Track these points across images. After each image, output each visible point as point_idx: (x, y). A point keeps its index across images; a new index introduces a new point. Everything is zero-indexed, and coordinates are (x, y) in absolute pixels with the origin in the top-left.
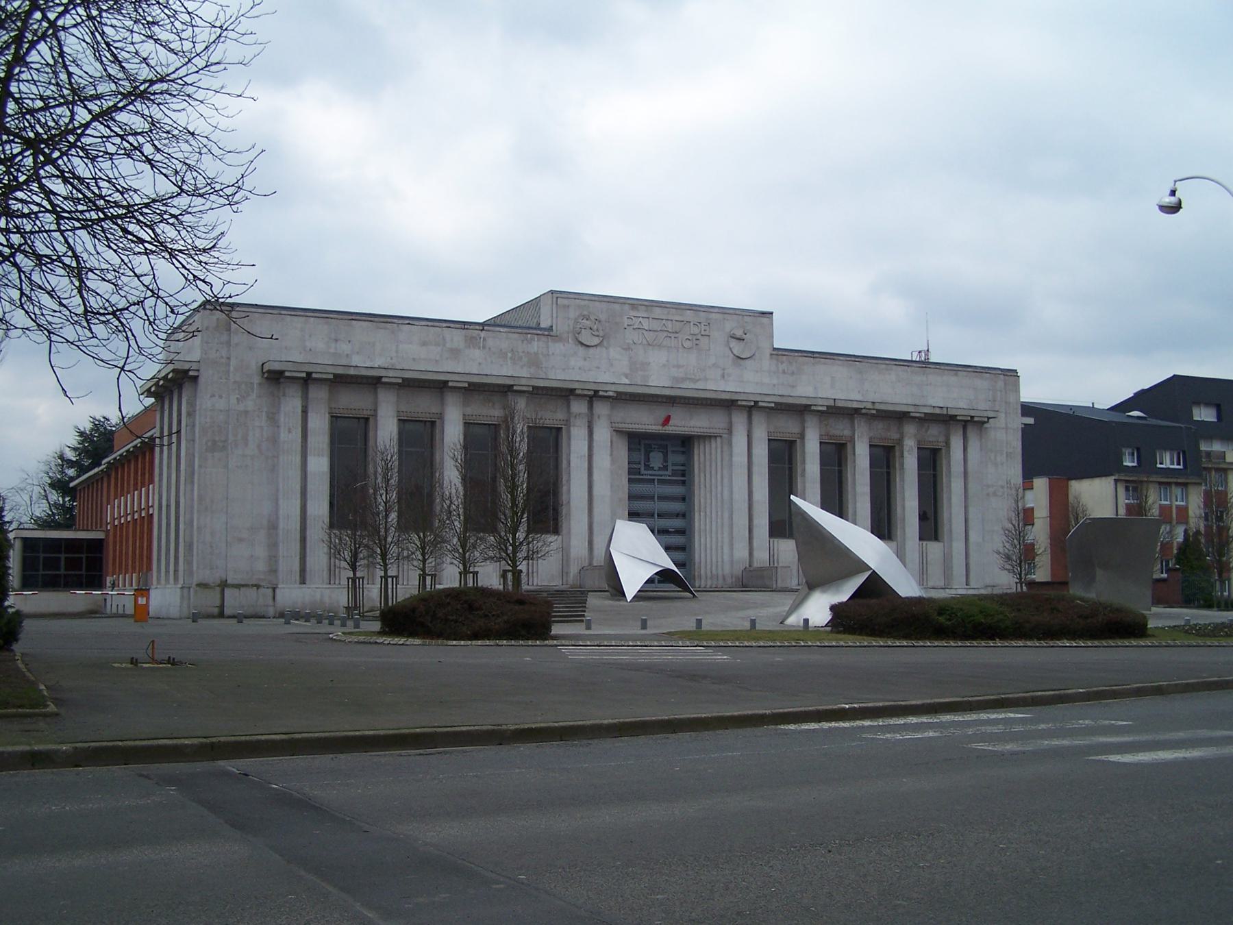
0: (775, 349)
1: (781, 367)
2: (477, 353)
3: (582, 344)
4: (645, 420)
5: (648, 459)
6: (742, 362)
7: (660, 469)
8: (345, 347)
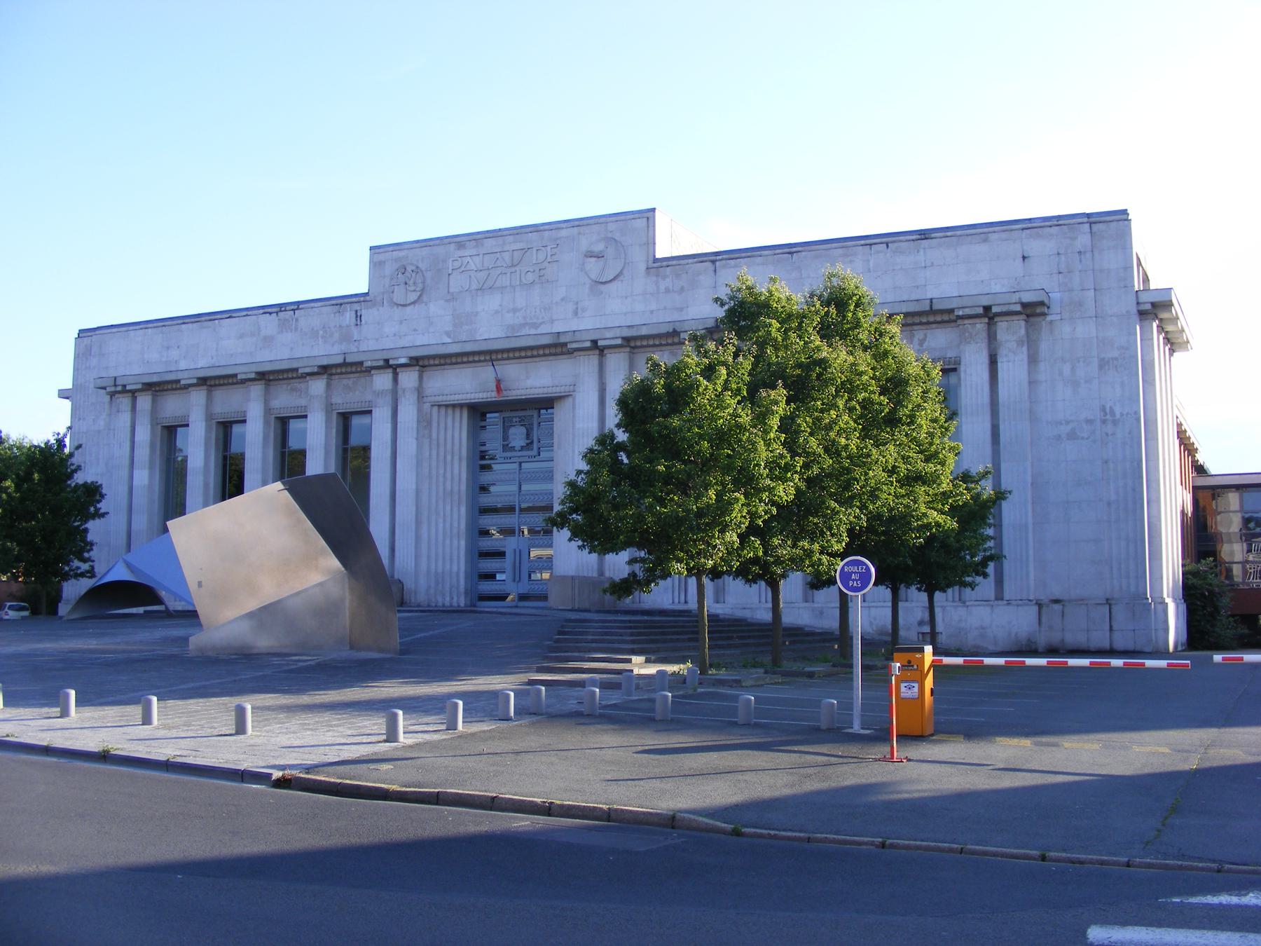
0: (656, 260)
1: (663, 285)
2: (288, 337)
3: (398, 305)
4: (468, 384)
5: (505, 438)
6: (602, 287)
7: (522, 448)
8: (174, 354)
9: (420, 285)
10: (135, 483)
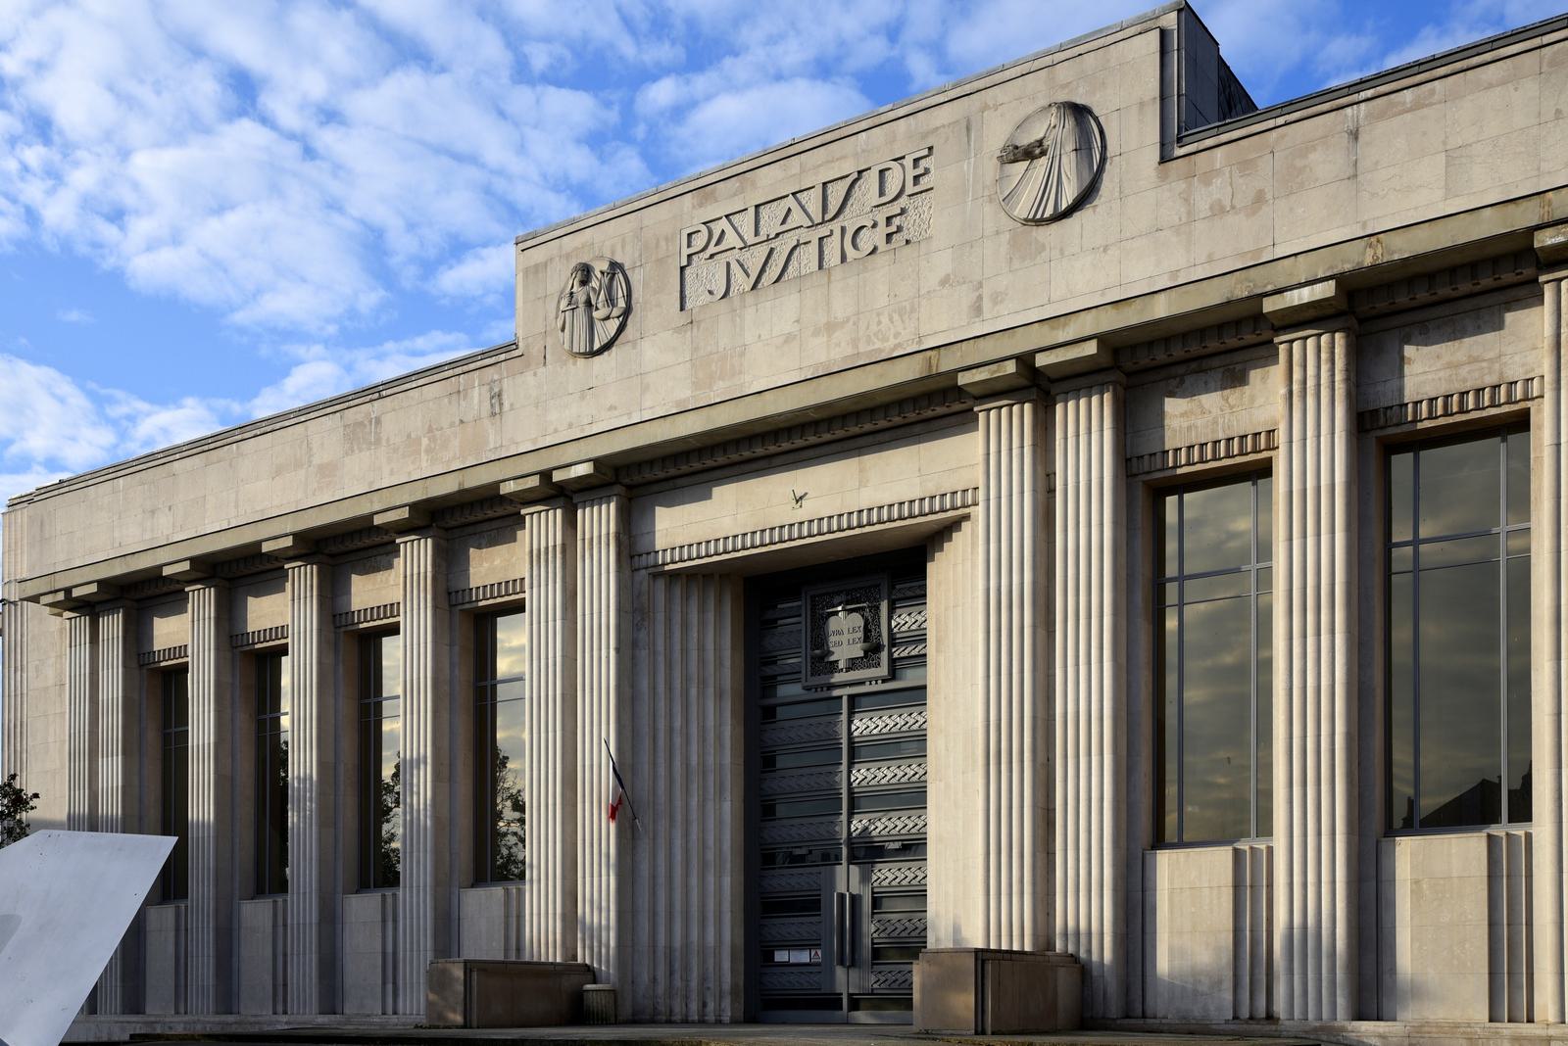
9: (622, 304)
10: (1423, 659)
